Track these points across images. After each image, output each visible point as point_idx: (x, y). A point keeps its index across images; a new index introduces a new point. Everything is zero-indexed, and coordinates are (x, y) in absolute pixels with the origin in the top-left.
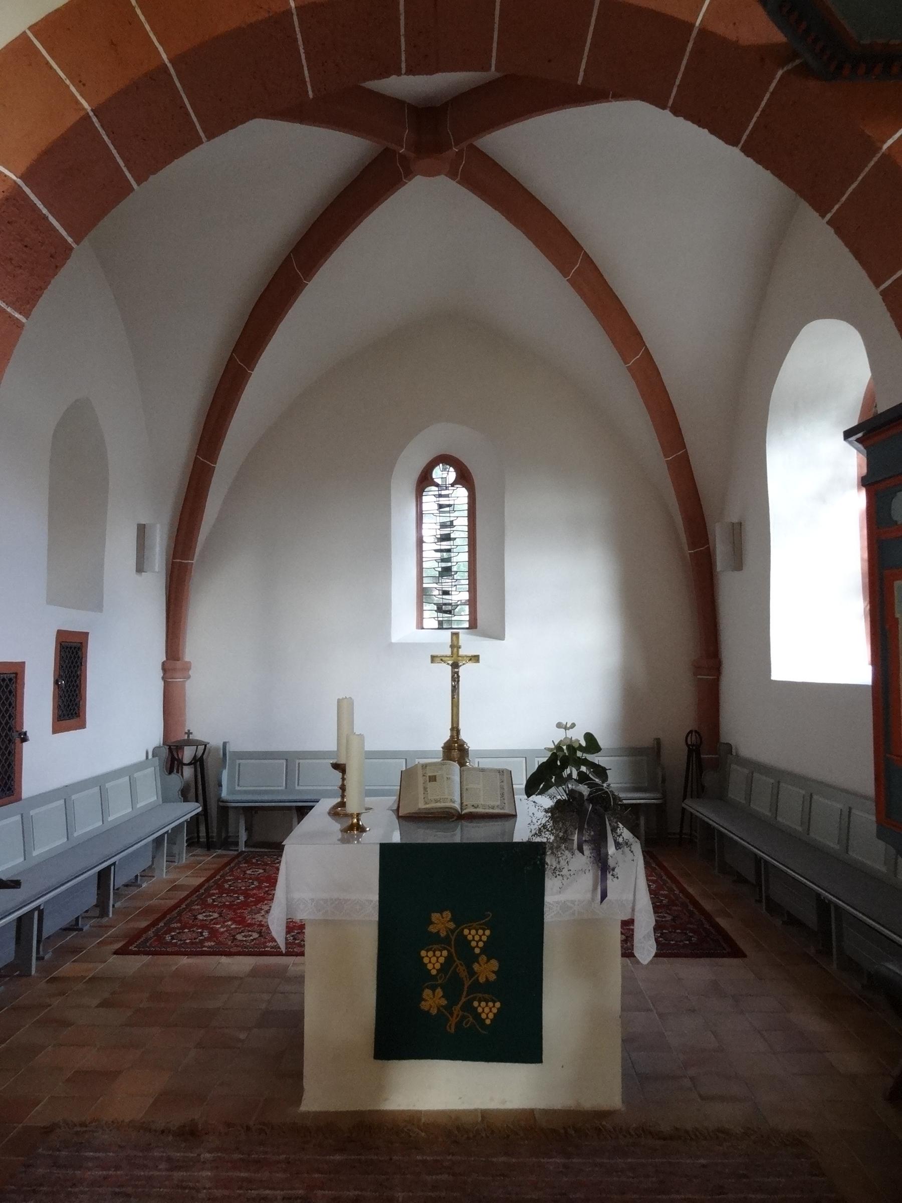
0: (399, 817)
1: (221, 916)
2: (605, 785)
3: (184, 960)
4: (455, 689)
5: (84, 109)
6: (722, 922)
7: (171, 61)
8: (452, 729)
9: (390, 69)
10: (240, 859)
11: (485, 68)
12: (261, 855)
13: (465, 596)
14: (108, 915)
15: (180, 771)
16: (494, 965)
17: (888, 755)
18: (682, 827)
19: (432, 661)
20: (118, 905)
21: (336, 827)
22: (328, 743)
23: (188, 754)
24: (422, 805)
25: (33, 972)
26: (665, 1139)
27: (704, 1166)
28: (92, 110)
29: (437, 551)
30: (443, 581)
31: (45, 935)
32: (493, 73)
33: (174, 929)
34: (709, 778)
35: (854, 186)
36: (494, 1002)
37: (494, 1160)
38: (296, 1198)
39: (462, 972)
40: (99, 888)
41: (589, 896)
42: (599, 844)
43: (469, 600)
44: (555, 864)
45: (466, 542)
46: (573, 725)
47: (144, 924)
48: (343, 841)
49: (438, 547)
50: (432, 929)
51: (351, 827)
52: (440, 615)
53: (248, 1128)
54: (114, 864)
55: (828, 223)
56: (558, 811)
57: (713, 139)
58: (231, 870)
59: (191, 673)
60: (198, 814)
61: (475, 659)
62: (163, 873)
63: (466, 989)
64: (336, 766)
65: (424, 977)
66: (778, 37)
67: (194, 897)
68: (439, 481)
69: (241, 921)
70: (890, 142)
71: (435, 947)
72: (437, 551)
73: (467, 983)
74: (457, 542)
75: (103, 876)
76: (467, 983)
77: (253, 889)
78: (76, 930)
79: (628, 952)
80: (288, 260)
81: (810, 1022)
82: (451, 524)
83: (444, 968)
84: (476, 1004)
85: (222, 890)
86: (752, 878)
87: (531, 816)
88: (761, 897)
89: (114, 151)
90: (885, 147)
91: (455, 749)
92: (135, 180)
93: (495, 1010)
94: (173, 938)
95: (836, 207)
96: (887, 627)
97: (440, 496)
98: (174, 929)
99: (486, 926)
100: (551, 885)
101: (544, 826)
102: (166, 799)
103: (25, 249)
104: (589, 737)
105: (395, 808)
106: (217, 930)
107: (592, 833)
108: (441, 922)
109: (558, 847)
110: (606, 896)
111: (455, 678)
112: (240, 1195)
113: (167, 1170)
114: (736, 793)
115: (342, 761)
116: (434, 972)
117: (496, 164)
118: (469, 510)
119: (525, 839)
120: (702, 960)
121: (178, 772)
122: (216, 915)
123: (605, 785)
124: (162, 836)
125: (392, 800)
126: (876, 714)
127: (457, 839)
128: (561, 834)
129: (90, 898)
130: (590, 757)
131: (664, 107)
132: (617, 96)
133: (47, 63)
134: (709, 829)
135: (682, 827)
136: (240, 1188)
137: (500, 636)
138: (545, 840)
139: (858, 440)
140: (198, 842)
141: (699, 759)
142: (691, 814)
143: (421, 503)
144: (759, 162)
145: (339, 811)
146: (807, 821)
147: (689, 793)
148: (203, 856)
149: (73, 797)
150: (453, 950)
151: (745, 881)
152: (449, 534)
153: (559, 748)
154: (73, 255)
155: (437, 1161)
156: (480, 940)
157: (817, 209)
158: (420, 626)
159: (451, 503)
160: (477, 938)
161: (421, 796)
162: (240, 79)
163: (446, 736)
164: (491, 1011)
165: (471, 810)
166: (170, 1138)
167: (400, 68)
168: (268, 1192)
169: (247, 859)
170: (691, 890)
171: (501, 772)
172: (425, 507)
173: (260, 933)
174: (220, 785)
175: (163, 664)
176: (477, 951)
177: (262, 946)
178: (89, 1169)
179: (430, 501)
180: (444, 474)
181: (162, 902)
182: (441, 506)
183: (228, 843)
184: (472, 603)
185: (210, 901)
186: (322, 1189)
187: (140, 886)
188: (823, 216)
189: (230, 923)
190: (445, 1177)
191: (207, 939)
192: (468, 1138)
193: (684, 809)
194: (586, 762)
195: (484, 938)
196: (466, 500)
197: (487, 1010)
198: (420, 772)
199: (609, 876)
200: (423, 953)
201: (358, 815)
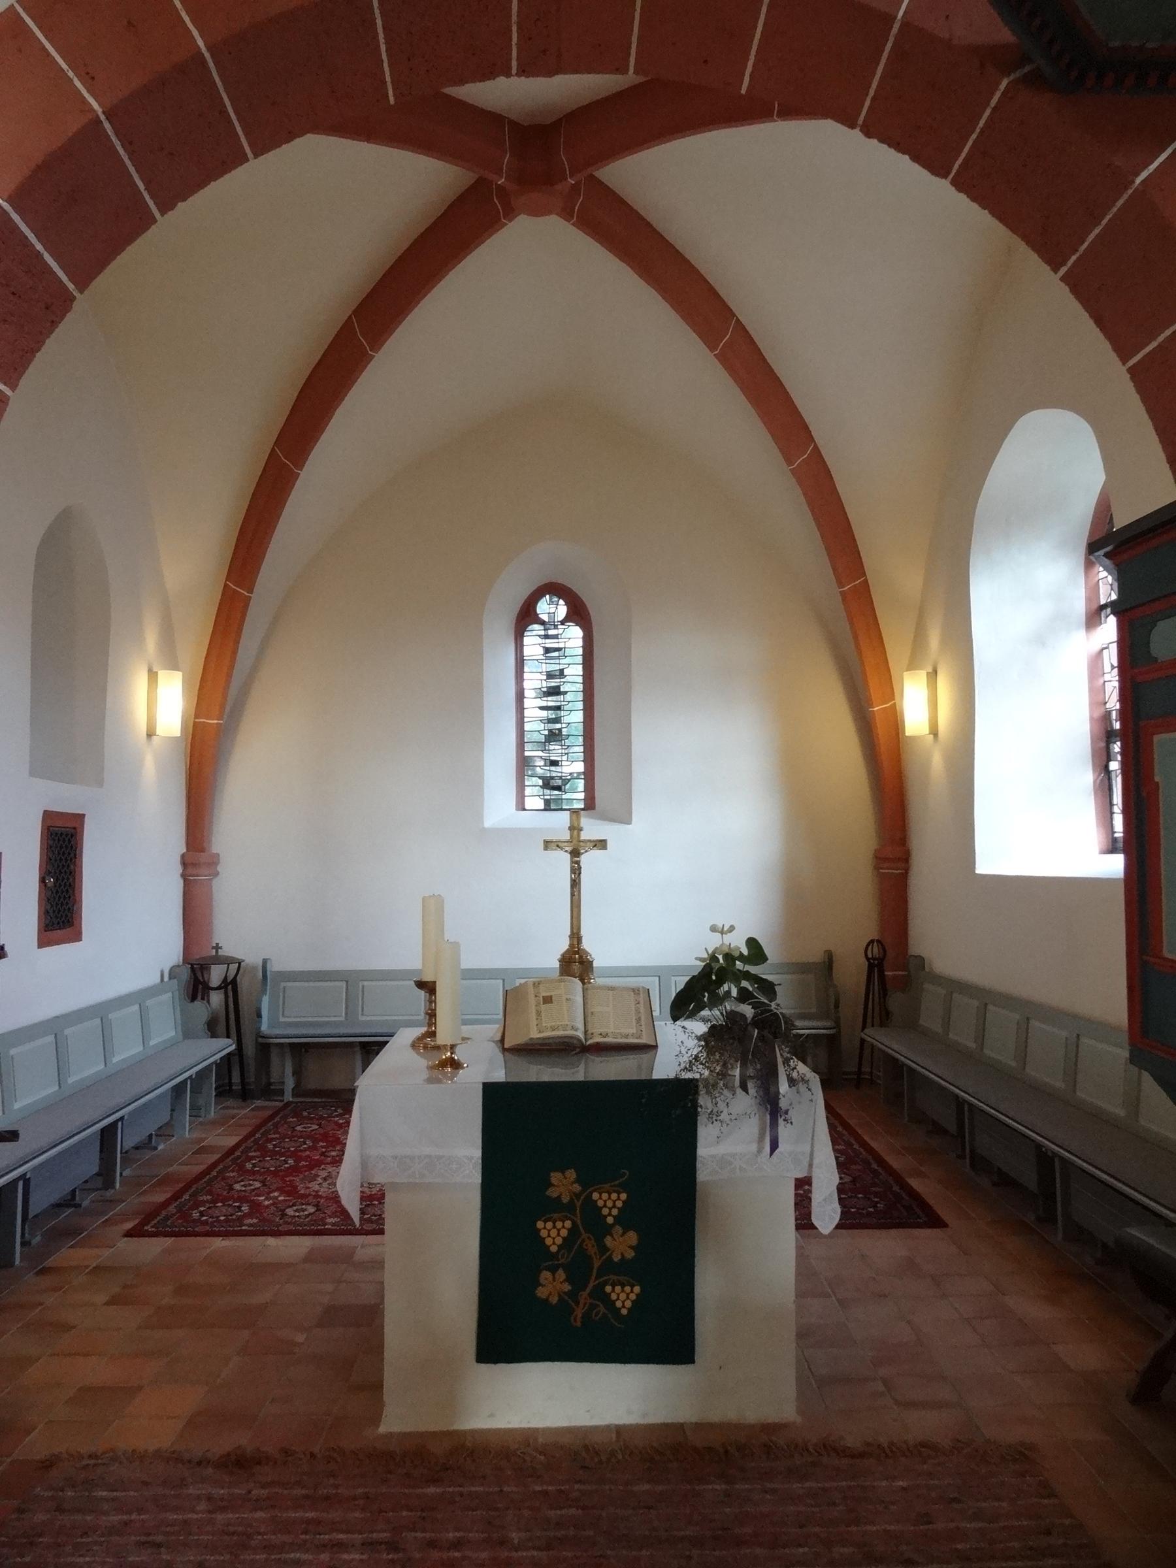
0: (504, 1050)
1: (264, 1185)
2: (773, 1005)
3: (219, 1243)
4: (575, 884)
5: (94, 111)
6: (914, 1183)
7: (209, 49)
8: (572, 937)
9: (494, 68)
10: (286, 1112)
11: (621, 69)
12: (315, 1106)
13: (579, 767)
14: (114, 1187)
15: (205, 997)
16: (632, 1238)
17: (1145, 957)
18: (860, 1064)
19: (546, 848)
20: (127, 1173)
21: (420, 1063)
22: (406, 954)
23: (216, 975)
24: (535, 1034)
25: (17, 1262)
26: (853, 1456)
27: (904, 1489)
28: (104, 112)
29: (542, 708)
30: (552, 747)
31: (33, 1211)
32: (630, 78)
33: (203, 1203)
34: (896, 1001)
35: (1097, 231)
36: (632, 1286)
37: (636, 1488)
38: (381, 1543)
39: (591, 1247)
40: (101, 1151)
41: (754, 1147)
42: (767, 1079)
43: (584, 773)
44: (710, 1106)
45: (580, 696)
46: (732, 929)
47: (160, 1197)
48: (430, 1080)
49: (544, 704)
50: (552, 1193)
51: (443, 1064)
52: (548, 792)
53: (312, 1455)
54: (122, 1118)
55: (1062, 279)
56: (714, 1039)
57: (916, 168)
58: (276, 1126)
59: (219, 869)
60: (229, 1054)
61: (601, 844)
62: (186, 1131)
63: (595, 1271)
64: (421, 985)
65: (541, 1256)
66: (1004, 35)
67: (228, 1161)
68: (545, 618)
69: (291, 1191)
70: (1144, 175)
71: (556, 1216)
72: (542, 708)
73: (597, 1264)
74: (568, 697)
75: (108, 1135)
76: (597, 1264)
77: (305, 1150)
78: (68, 1206)
79: (804, 1223)
80: (347, 326)
81: (1032, 1307)
82: (561, 673)
83: (568, 1242)
84: (608, 1289)
85: (264, 1152)
86: (952, 1128)
87: (677, 1047)
88: (964, 1149)
89: (132, 169)
90: (1138, 180)
91: (576, 962)
92: (158, 209)
93: (633, 1297)
94: (202, 1214)
95: (1074, 258)
96: (1144, 794)
97: (547, 637)
98: (203, 1203)
99: (624, 1187)
100: (706, 1133)
101: (696, 1058)
102: (188, 1033)
103: (12, 297)
104: (752, 943)
105: (498, 1037)
106: (259, 1204)
107: (758, 1066)
108: (563, 1184)
109: (715, 1085)
110: (777, 1147)
111: (576, 870)
112: (305, 1541)
113: (210, 1512)
114: (930, 1020)
115: (428, 978)
116: (554, 1249)
117: (622, 202)
118: (584, 656)
119: (672, 1076)
120: (893, 1232)
121: (203, 999)
122: (257, 1184)
123: (773, 1005)
124: (184, 1082)
125: (494, 1030)
126: (1128, 903)
127: (580, 1077)
128: (718, 1068)
129: (90, 1165)
130: (753, 970)
131: (852, 126)
132: (790, 112)
133: (44, 49)
134: (896, 1068)
135: (860, 1064)
136: (306, 1532)
137: (627, 820)
138: (697, 1076)
139: (1106, 555)
140: (230, 1090)
141: (882, 977)
142: (872, 1046)
143: (522, 646)
144: (974, 199)
145: (426, 1043)
146: (1022, 1054)
147: (869, 1020)
148: (238, 1108)
149: (67, 1032)
150: (579, 1222)
151: (945, 1132)
152: (558, 687)
153: (713, 958)
154: (76, 305)
155: (561, 1491)
156: (614, 1206)
157: (1049, 262)
158: (521, 806)
159: (561, 645)
160: (610, 1204)
161: (533, 1022)
162: (293, 81)
163: (564, 945)
164: (628, 1298)
165: (597, 1039)
166: (210, 1470)
167: (510, 68)
168: (341, 1536)
169: (296, 1111)
170: (874, 1144)
171: (636, 991)
172: (527, 651)
173: (317, 1206)
174: (259, 1016)
175: (183, 856)
176: (610, 1220)
177: (328, 1219)
178: (106, 1513)
179: (533, 643)
180: (551, 609)
181: (185, 1168)
182: (547, 650)
183: (269, 1091)
184: (589, 775)
185: (249, 1166)
186: (414, 1530)
187: (156, 1148)
188: (1055, 270)
189: (276, 1194)
190: (573, 1511)
191: (246, 1216)
192: (601, 1462)
193: (863, 1041)
194: (747, 976)
195: (619, 1204)
196: (580, 643)
197: (623, 1296)
198: (531, 991)
199: (781, 1121)
200: (540, 1224)
201: (453, 1047)
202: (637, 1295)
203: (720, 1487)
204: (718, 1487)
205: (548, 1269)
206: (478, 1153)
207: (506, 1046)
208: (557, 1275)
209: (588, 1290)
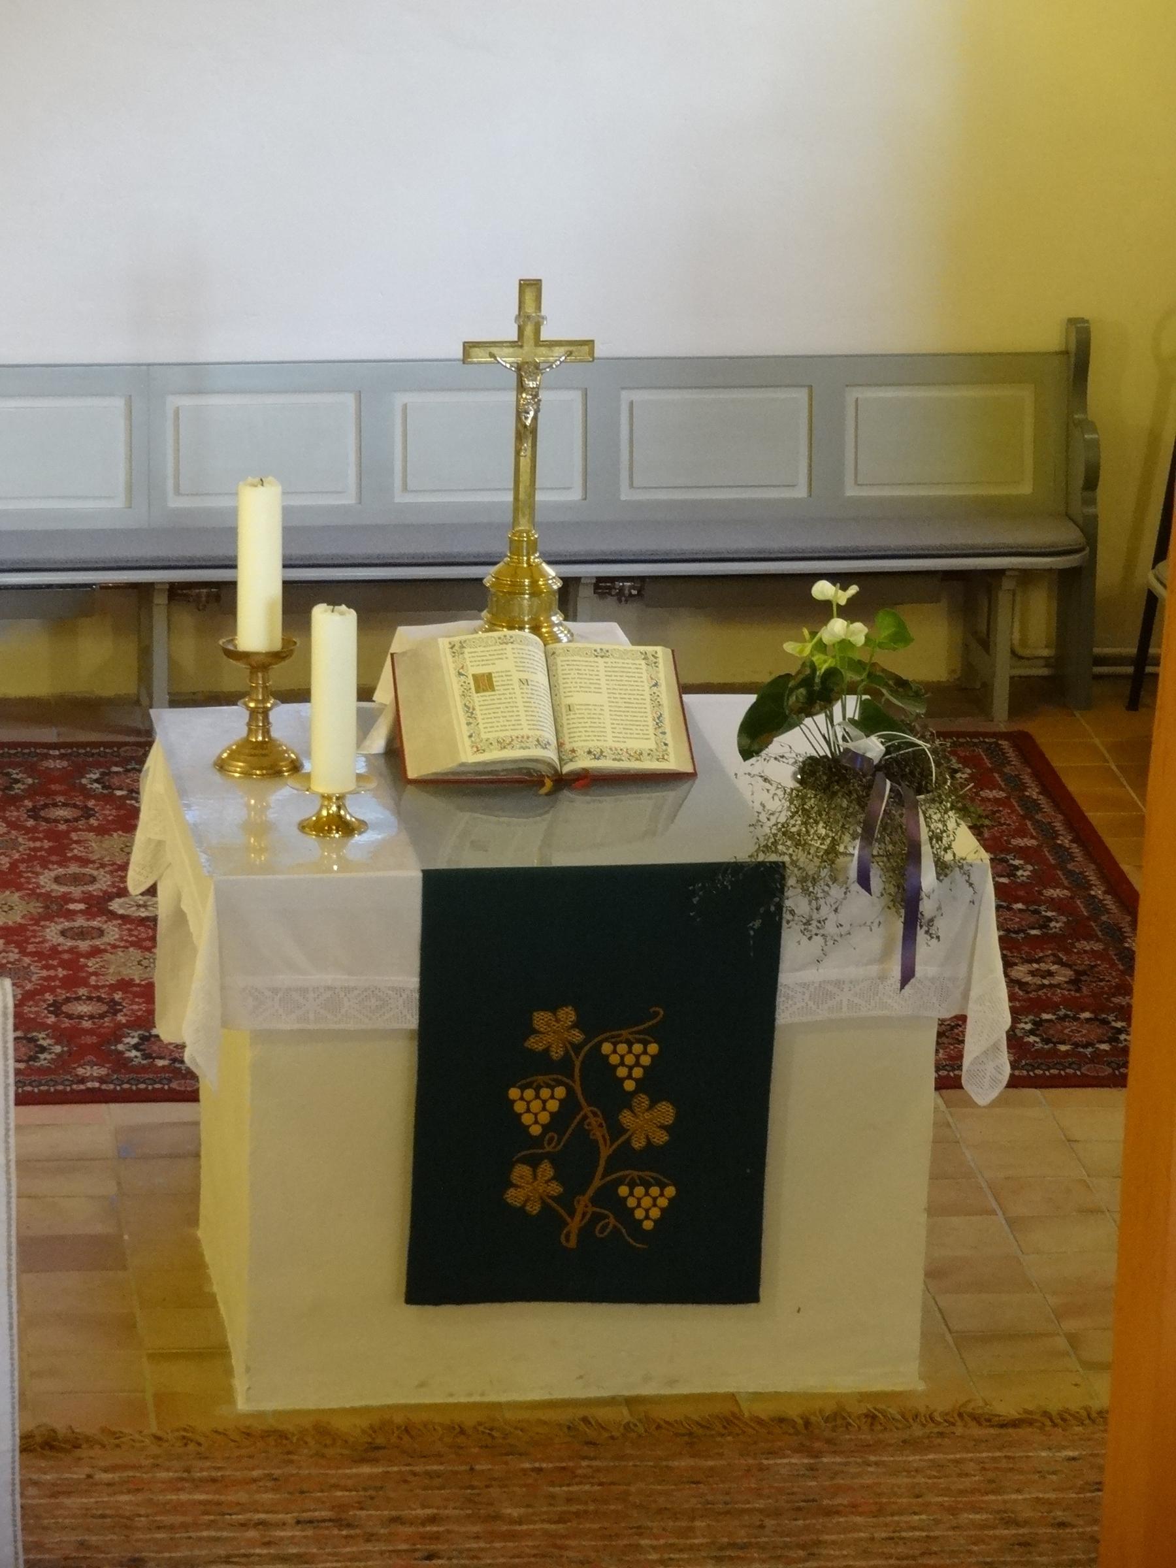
16: (666, 1112)
24: (468, 757)
26: (1002, 1426)
36: (662, 1187)
50: (534, 1043)
61: (530, 288)
63: (602, 1163)
65: (513, 1141)
71: (541, 1079)
73: (605, 1152)
76: (605, 1152)
79: (948, 1078)
83: (558, 1122)
84: (623, 1190)
93: (663, 1202)
100: (795, 948)
108: (554, 1030)
116: (536, 1130)
176: (629, 1086)
197: (646, 1202)
200: (514, 1093)
202: (671, 1200)
203: (799, 1460)
204: (793, 1461)
205: (524, 1161)
206: (413, 982)
207: (413, 771)
208: (540, 1171)
209: (590, 1192)
